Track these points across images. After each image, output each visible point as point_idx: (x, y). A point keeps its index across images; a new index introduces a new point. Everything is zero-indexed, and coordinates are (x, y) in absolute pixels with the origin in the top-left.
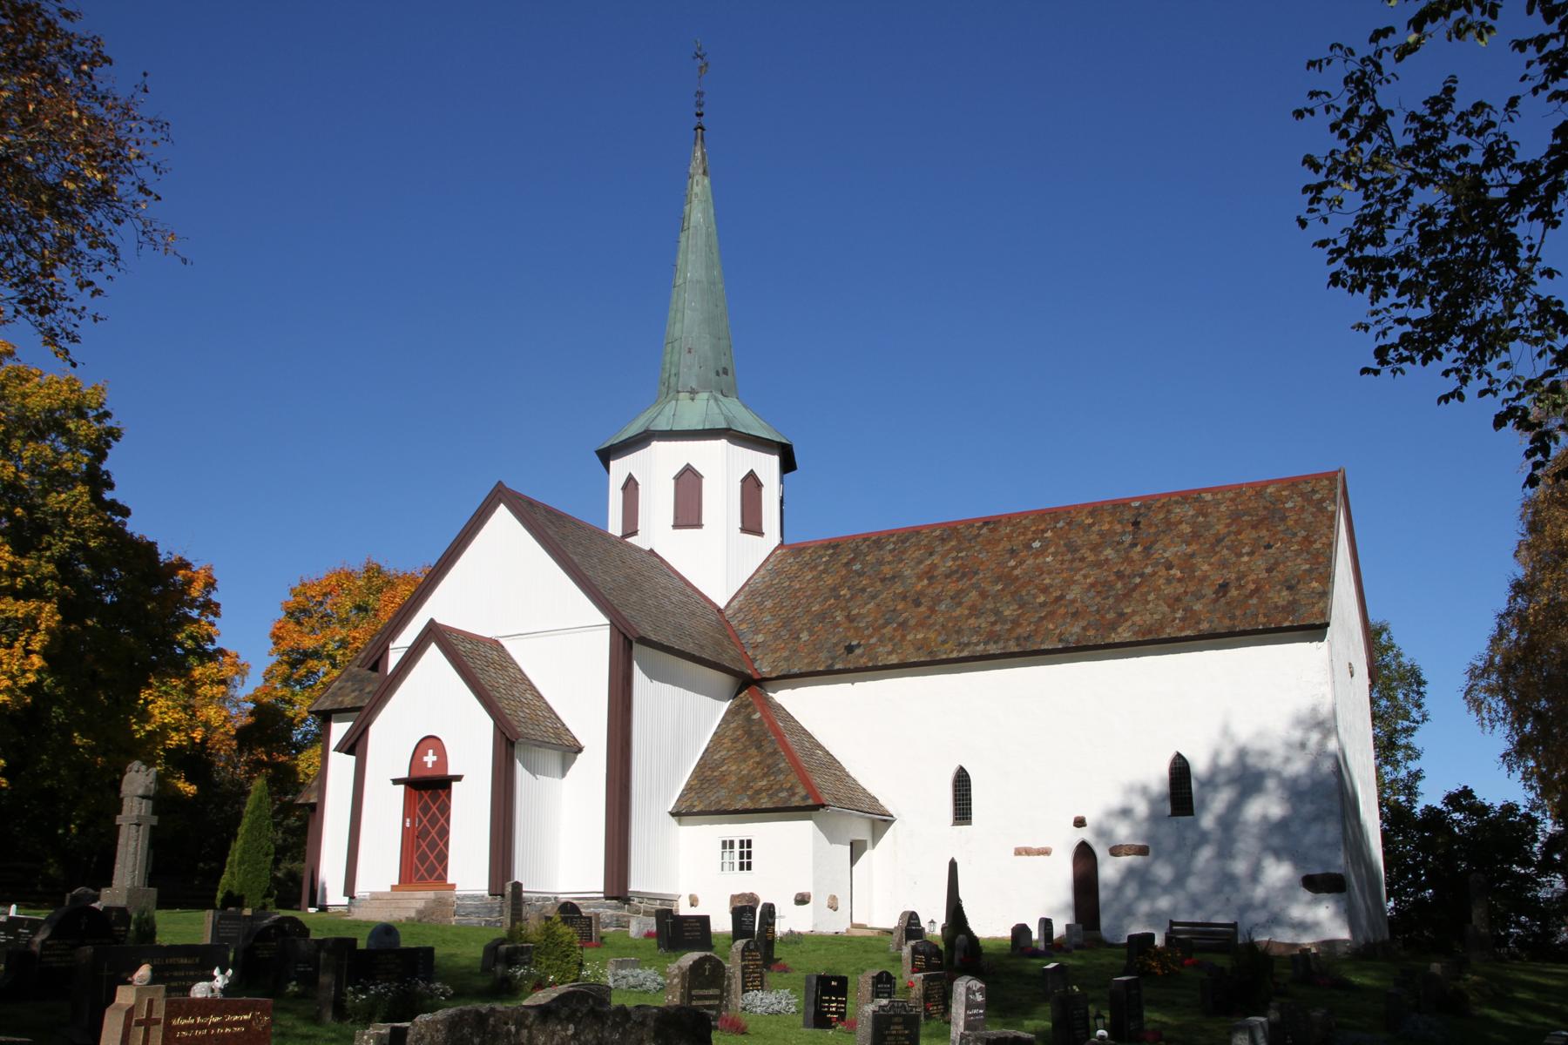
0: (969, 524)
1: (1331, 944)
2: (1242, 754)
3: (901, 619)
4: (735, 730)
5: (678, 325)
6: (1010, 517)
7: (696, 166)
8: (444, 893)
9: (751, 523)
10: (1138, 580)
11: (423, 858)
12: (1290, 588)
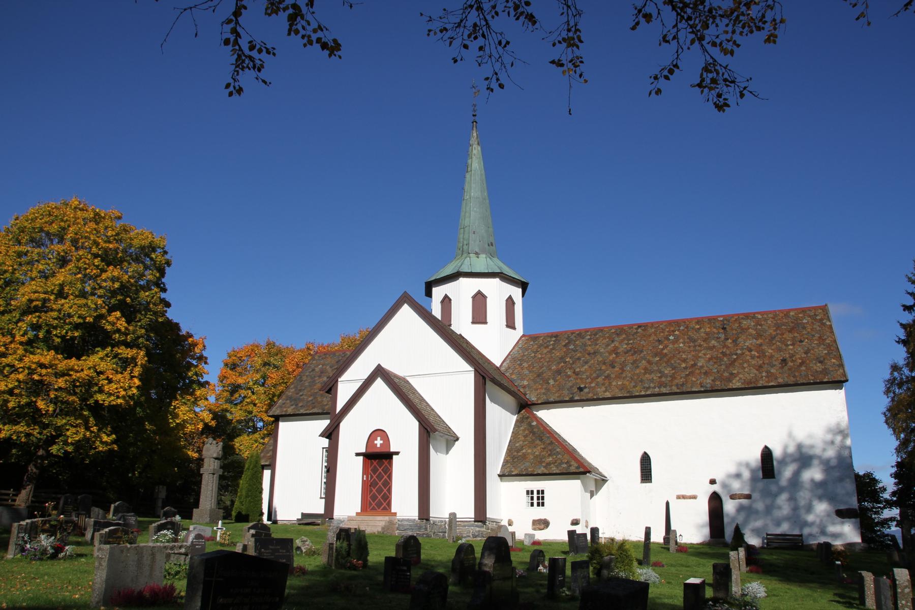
0: (630, 326)
1: (850, 545)
2: (800, 447)
3: (606, 374)
4: (524, 430)
5: (467, 220)
6: (652, 324)
7: (474, 140)
8: (392, 518)
9: (511, 324)
10: (735, 357)
11: (374, 498)
12: (821, 362)
